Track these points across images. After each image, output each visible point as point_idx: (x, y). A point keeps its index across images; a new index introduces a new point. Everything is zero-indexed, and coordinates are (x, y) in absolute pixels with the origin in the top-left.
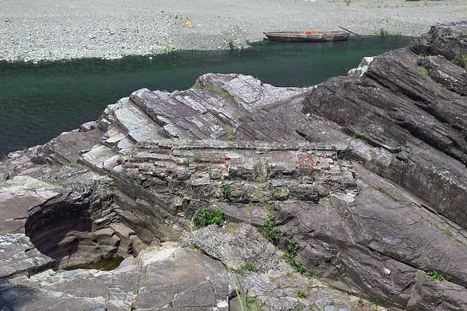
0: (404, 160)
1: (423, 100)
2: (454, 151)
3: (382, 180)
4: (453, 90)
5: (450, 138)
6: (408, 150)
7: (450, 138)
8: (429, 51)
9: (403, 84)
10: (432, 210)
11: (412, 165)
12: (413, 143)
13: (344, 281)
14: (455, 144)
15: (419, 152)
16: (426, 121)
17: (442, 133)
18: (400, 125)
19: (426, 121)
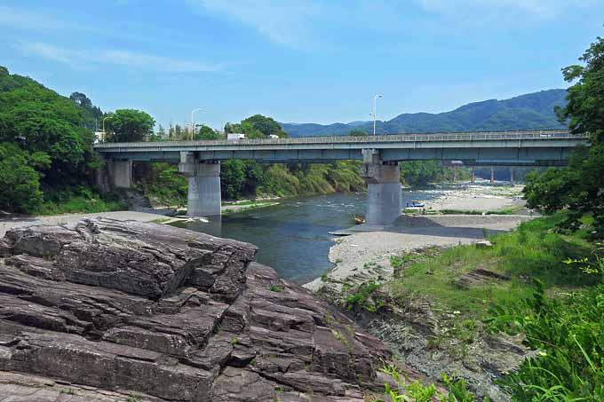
0: (27, 347)
1: (26, 292)
2: (68, 327)
3: (8, 374)
4: (49, 279)
5: (63, 318)
6: (27, 338)
7: (63, 318)
8: (13, 251)
9: (429, 192)
10: (129, 360)
11: (37, 349)
12: (28, 331)
13: (283, 321)
14: (69, 322)
15: (32, 336)
16: (34, 309)
17: (53, 315)
18: (9, 319)
19: (34, 309)
